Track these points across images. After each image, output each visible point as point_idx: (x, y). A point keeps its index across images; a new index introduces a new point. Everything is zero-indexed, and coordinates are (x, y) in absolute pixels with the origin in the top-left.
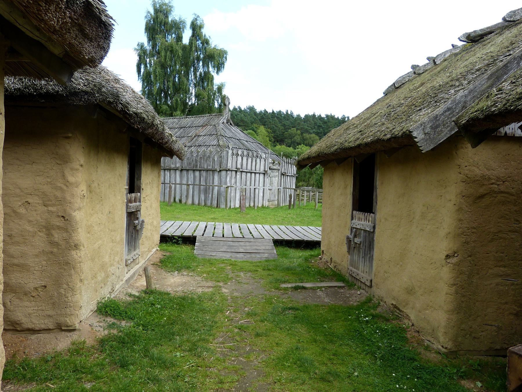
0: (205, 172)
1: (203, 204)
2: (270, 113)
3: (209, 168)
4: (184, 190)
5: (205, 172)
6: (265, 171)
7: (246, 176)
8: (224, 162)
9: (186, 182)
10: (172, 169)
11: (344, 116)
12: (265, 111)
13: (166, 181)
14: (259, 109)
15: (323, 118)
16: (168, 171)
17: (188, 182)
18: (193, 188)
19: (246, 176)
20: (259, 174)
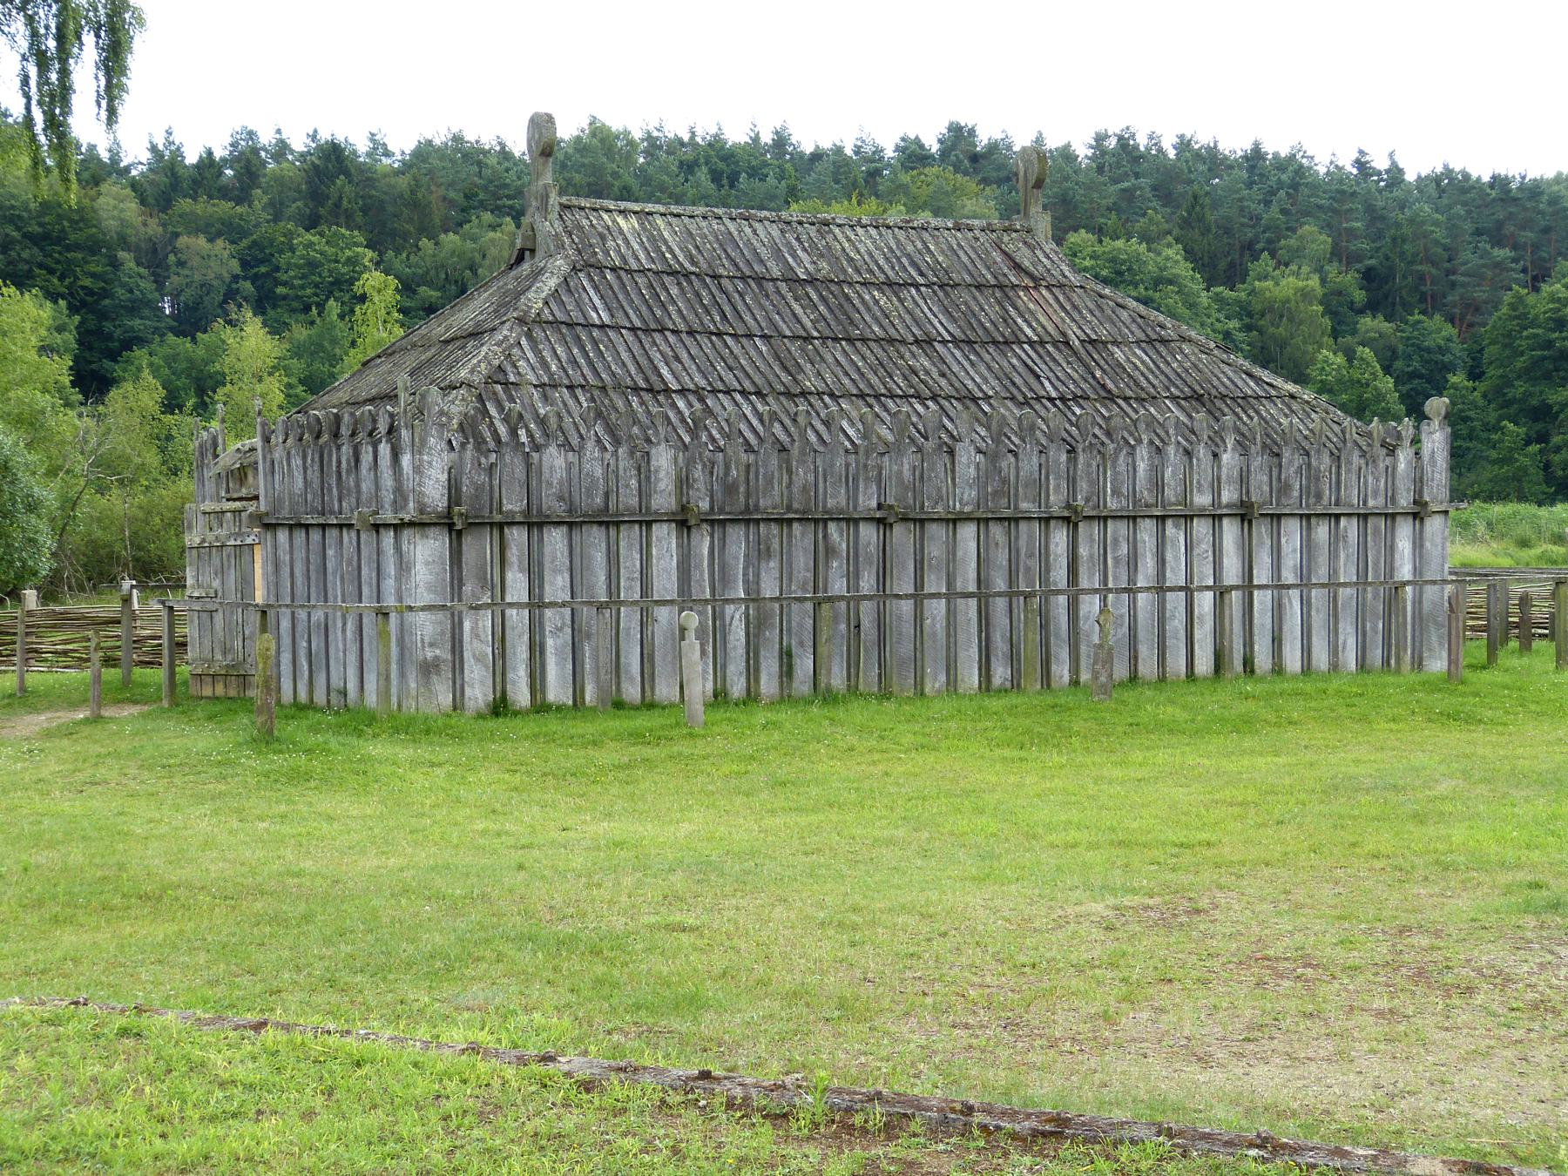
0: (1355, 521)
1: (1353, 666)
2: (766, 144)
3: (1371, 503)
4: (1262, 612)
5: (1355, 521)
6: (1068, 506)
7: (308, 539)
8: (1437, 476)
9: (912, 586)
10: (1199, 516)
11: (1182, 137)
12: (781, 141)
13: (1168, 574)
14: (806, 140)
15: (847, 161)
16: (1176, 526)
17: (919, 583)
18: (1306, 603)
19: (308, 539)
20: (564, 529)
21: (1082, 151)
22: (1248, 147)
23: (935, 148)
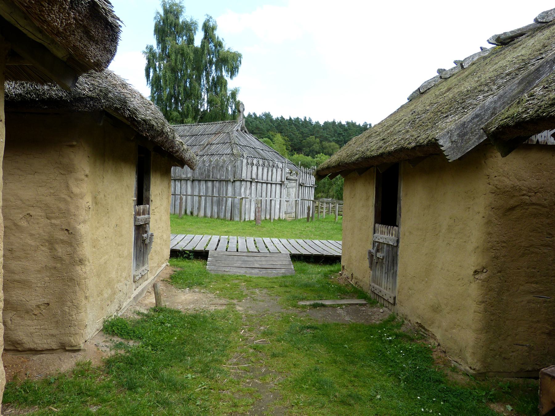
0: (218, 182)
1: (216, 216)
2: (287, 120)
3: (222, 178)
4: (196, 202)
5: (218, 182)
6: (281, 181)
7: (262, 187)
8: (239, 171)
9: (198, 193)
10: (183, 180)
11: (365, 123)
12: (282, 117)
13: (176, 192)
14: (275, 116)
15: (343, 126)
16: (178, 182)
17: (199, 193)
18: (205, 200)
19: (262, 187)
20: (275, 185)
21: (286, 119)
22: (332, 121)
23: (246, 117)
